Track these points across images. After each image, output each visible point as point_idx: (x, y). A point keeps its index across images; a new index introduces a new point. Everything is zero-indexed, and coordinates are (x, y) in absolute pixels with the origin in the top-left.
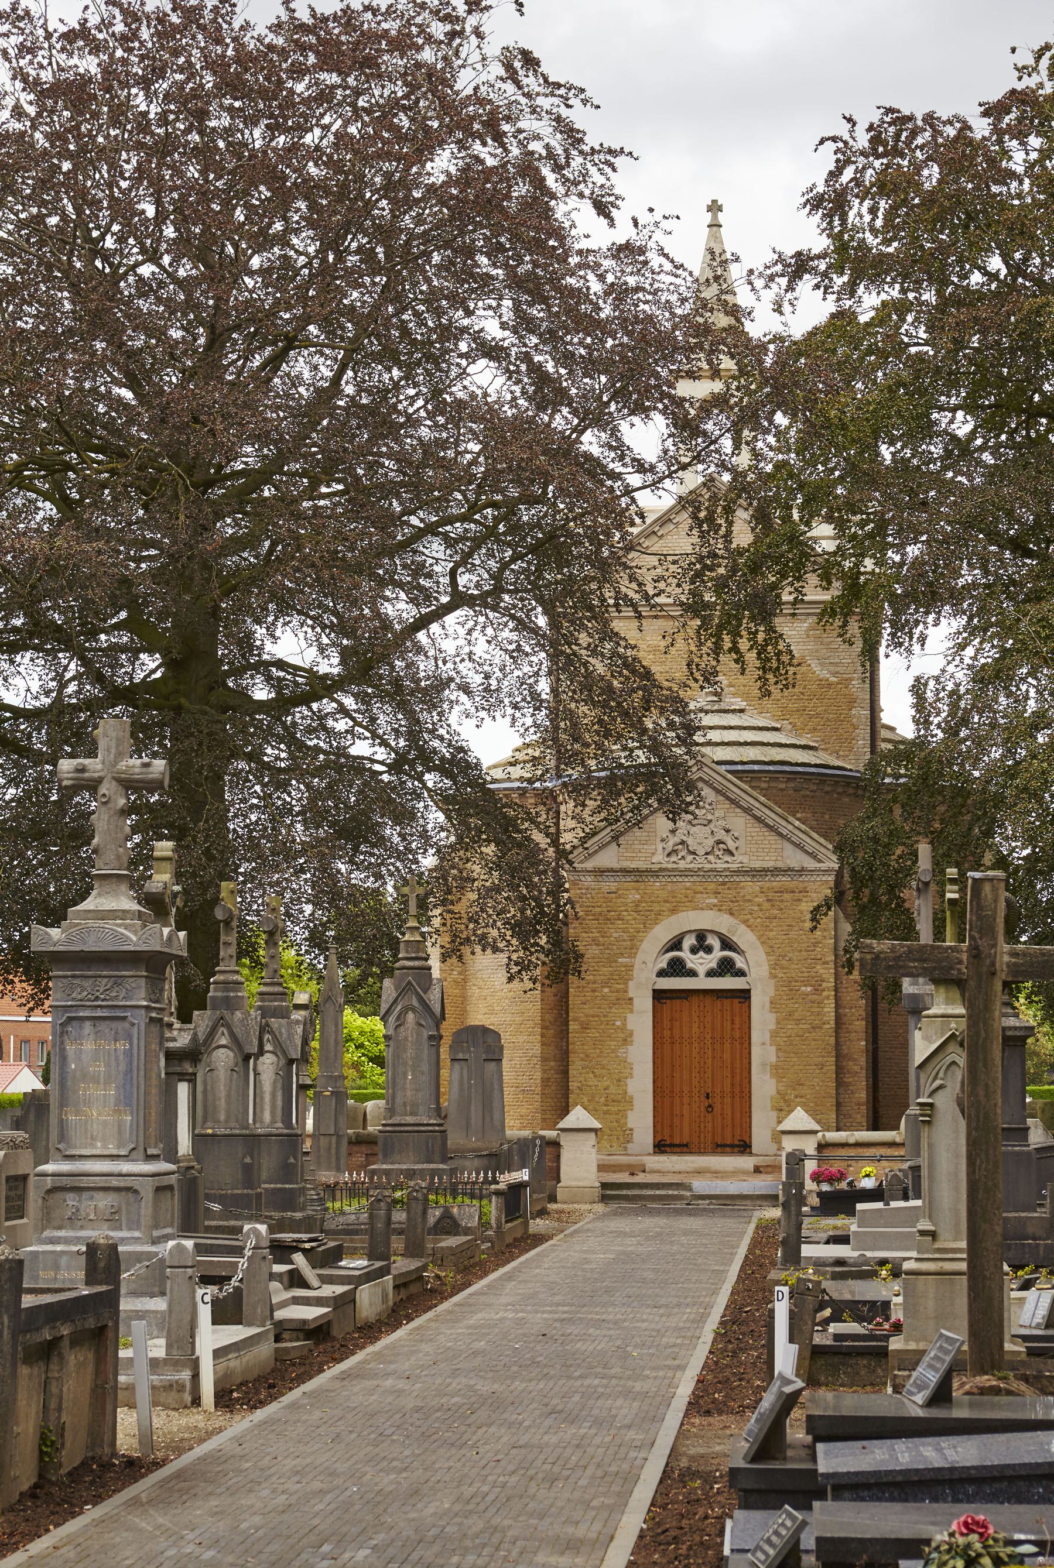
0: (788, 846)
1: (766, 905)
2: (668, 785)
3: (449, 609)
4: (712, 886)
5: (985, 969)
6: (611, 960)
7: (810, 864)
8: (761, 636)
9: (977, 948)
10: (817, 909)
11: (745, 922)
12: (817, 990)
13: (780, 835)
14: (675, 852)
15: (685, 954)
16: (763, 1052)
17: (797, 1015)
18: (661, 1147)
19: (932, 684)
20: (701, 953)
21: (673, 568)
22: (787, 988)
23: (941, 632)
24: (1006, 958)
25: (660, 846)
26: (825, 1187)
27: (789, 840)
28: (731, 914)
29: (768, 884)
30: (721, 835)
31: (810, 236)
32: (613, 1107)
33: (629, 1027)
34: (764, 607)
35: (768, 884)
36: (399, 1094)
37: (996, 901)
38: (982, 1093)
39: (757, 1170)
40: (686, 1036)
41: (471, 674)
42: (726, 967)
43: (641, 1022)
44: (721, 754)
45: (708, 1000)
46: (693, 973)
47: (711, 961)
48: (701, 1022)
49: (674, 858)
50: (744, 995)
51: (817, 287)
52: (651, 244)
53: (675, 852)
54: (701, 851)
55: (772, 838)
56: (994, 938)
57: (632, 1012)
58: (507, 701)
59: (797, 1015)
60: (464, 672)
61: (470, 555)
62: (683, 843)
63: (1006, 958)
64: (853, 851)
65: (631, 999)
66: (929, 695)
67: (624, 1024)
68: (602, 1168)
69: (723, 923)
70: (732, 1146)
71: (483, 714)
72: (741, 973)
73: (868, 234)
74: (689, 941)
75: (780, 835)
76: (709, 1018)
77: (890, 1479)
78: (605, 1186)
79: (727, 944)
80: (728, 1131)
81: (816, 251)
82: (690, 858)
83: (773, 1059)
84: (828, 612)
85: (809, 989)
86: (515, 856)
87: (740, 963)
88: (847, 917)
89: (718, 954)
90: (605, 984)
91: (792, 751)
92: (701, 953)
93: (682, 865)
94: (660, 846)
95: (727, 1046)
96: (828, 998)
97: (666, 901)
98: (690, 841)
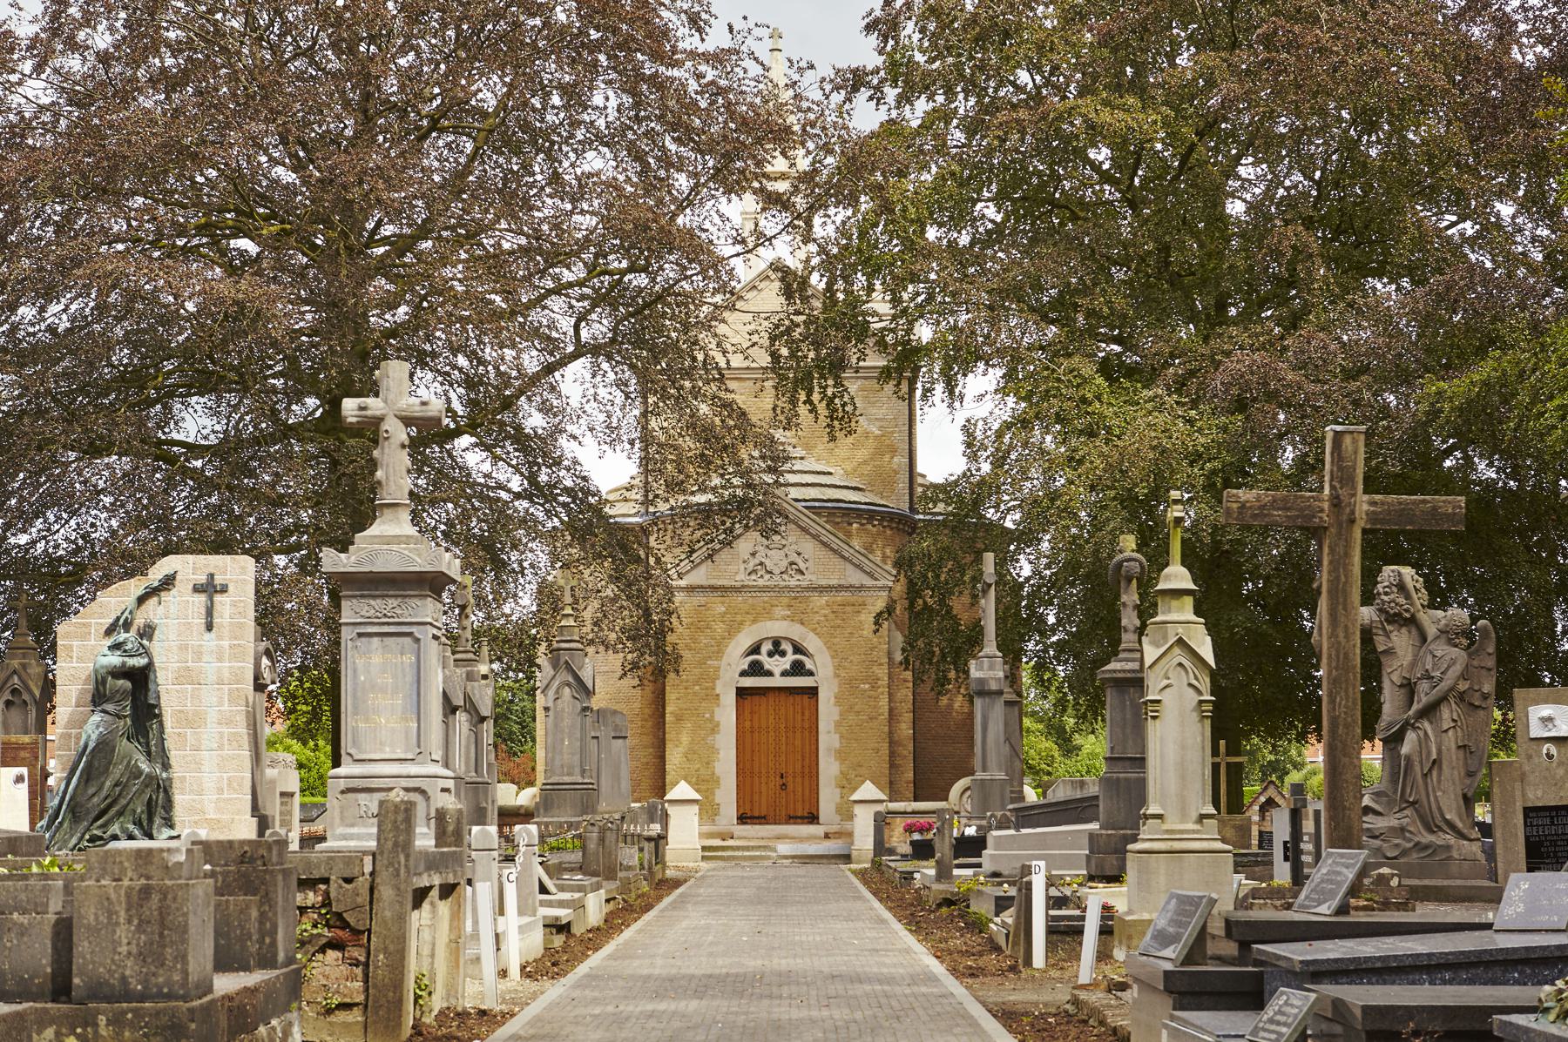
0: (850, 567)
1: (832, 616)
2: (754, 511)
3: (575, 356)
4: (786, 600)
5: (1345, 517)
6: (702, 663)
7: (869, 582)
8: (830, 392)
9: (1337, 497)
10: (879, 615)
11: (814, 630)
12: (874, 687)
13: (843, 557)
14: (755, 571)
16: (828, 738)
17: (857, 708)
18: (743, 819)
19: (980, 423)
21: (766, 323)
22: (849, 687)
23: (981, 382)
24: (1365, 507)
25: (742, 567)
26: (916, 837)
27: (850, 561)
30: (794, 557)
31: (867, 54)
32: (706, 784)
34: (836, 366)
36: (558, 757)
37: (1356, 453)
38: (1342, 635)
39: (827, 836)
40: (764, 725)
41: (596, 413)
42: (797, 669)
43: (727, 713)
44: (794, 493)
45: (783, 697)
46: (769, 674)
47: (785, 663)
48: (777, 714)
49: (753, 577)
50: (813, 692)
51: (871, 98)
52: (744, 48)
53: (755, 571)
54: (777, 571)
55: (836, 560)
56: (1354, 488)
58: (625, 438)
59: (857, 708)
60: (589, 411)
61: (589, 312)
62: (761, 564)
63: (1365, 507)
64: (911, 566)
66: (978, 433)
67: (712, 716)
68: (701, 835)
69: (795, 631)
70: (802, 818)
71: (605, 447)
72: (811, 674)
73: (916, 53)
75: (843, 557)
76: (783, 711)
77: (1370, 965)
78: (704, 848)
79: (798, 649)
80: (799, 806)
81: (870, 68)
82: (767, 577)
83: (837, 745)
84: (885, 374)
86: (632, 570)
87: (809, 665)
88: (898, 628)
89: (791, 657)
90: (697, 683)
91: (845, 492)
93: (761, 582)
94: (742, 567)
95: (798, 735)
98: (767, 562)
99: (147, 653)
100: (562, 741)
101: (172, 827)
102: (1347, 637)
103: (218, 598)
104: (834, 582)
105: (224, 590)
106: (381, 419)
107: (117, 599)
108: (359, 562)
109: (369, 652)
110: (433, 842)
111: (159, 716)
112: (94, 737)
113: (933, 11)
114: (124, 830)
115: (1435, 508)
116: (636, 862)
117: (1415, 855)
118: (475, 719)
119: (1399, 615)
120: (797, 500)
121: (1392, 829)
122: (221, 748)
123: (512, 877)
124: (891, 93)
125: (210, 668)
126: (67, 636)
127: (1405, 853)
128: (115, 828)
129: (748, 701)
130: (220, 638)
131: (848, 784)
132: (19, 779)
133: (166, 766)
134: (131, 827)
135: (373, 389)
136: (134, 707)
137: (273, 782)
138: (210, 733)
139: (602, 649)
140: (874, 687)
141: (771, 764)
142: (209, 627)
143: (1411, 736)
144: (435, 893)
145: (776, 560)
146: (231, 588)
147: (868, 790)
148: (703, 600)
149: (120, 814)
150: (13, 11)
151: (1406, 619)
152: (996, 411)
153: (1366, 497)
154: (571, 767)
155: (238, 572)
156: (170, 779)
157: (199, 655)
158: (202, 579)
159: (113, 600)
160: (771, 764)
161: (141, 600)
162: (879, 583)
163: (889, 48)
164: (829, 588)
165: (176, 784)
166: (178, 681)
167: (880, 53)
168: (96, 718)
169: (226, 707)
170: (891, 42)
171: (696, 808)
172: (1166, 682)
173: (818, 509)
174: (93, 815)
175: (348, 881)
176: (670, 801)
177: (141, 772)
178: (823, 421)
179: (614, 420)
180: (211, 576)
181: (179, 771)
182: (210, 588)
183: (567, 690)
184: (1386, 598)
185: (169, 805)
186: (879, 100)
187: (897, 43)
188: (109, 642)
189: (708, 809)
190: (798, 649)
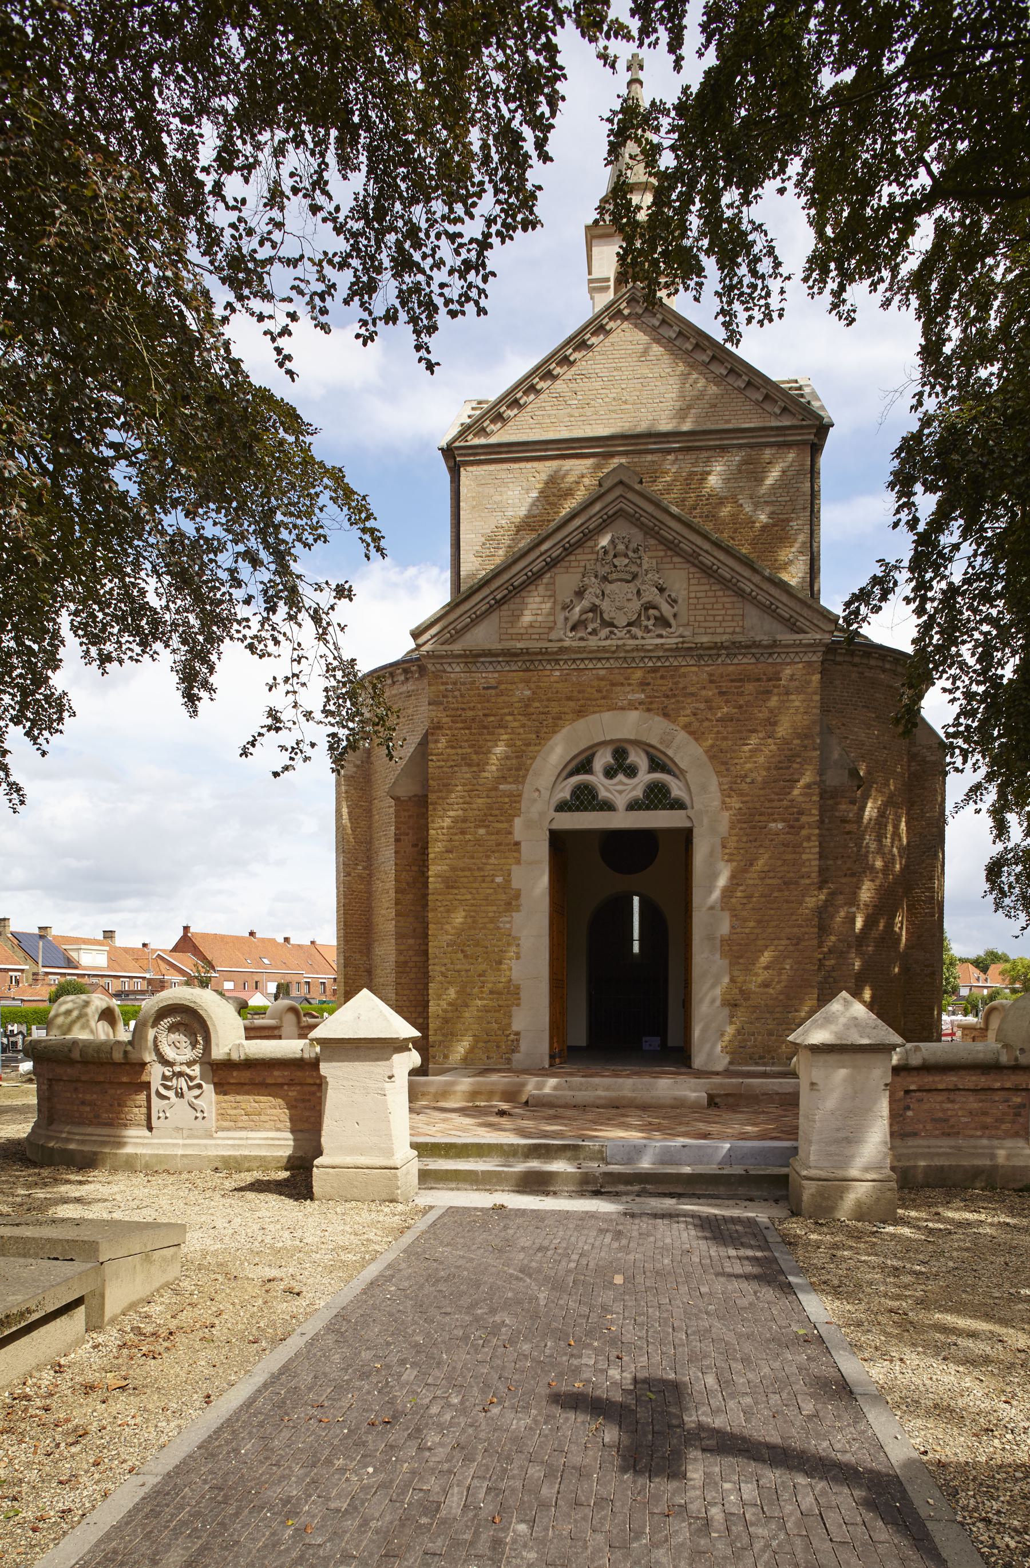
4: (639, 674)
7: (787, 637)
12: (794, 828)
15: (597, 779)
20: (621, 777)
22: (750, 825)
27: (753, 601)
28: (666, 715)
29: (721, 669)
30: (651, 594)
33: (515, 884)
35: (721, 669)
42: (657, 797)
47: (634, 787)
50: (685, 837)
54: (622, 621)
57: (518, 862)
62: (594, 609)
65: (517, 844)
67: (508, 881)
72: (678, 805)
74: (603, 759)
75: (740, 594)
85: (780, 826)
87: (676, 790)
89: (645, 777)
92: (621, 777)
93: (593, 642)
96: (808, 839)
97: (569, 699)
98: (605, 605)
145: (621, 601)
148: (492, 678)
162: (807, 638)
190: (656, 765)
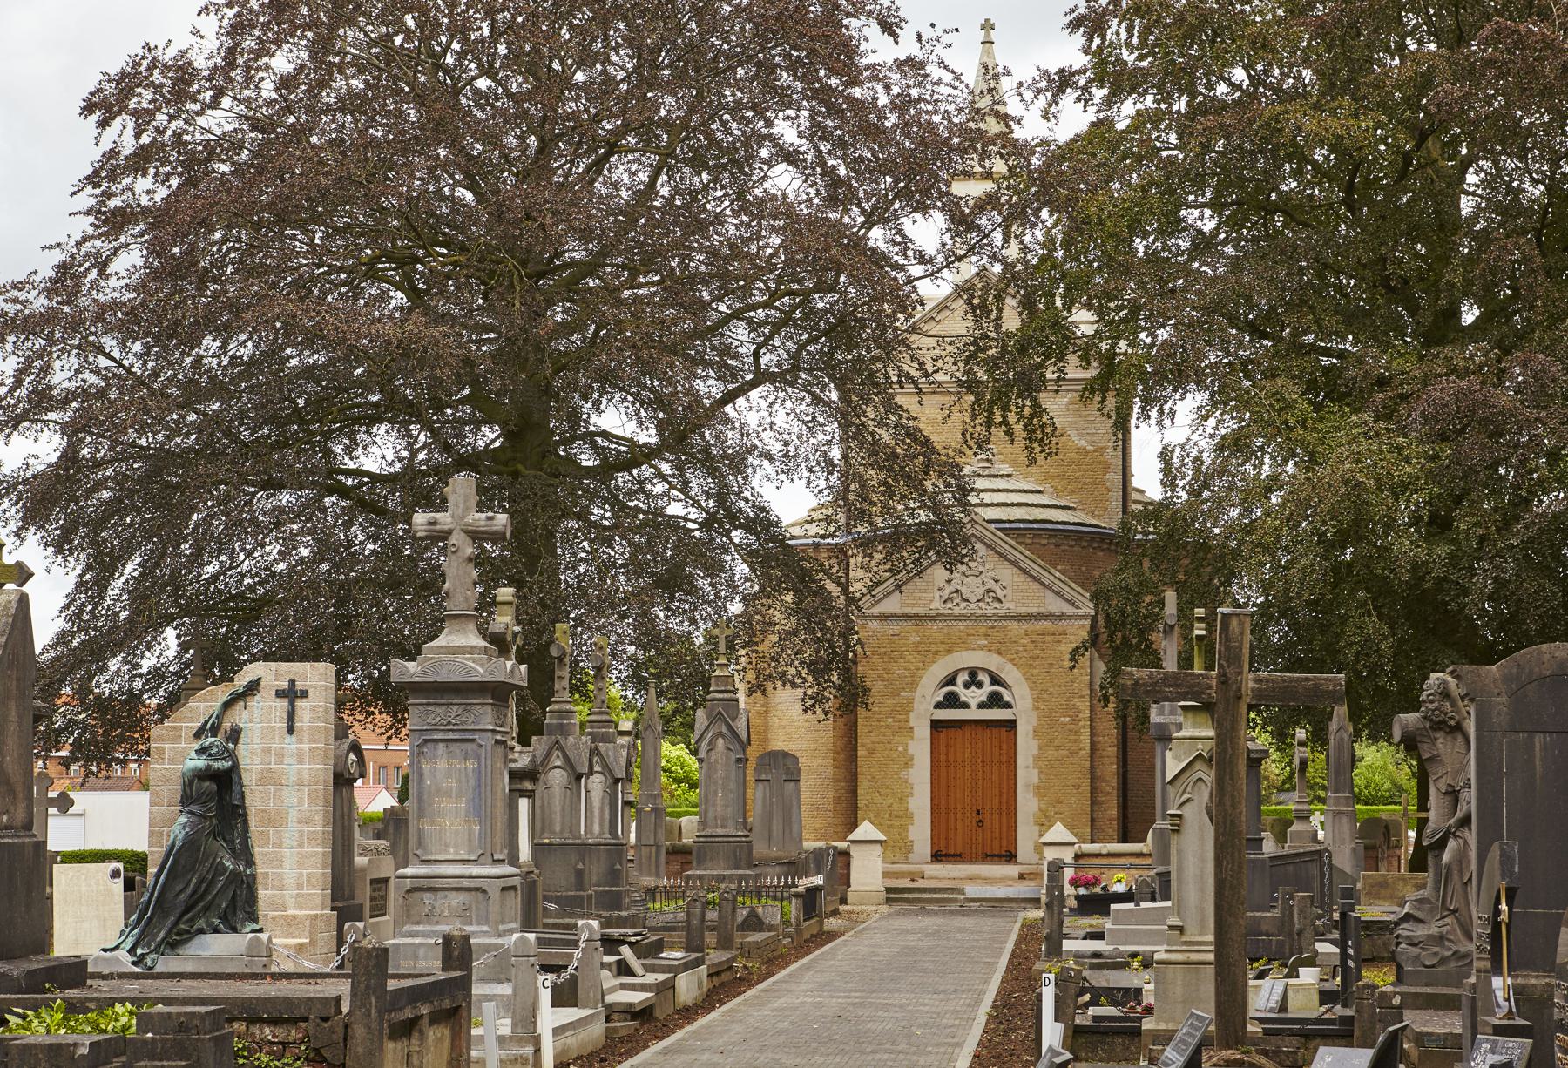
0: (1049, 594)
1: (1030, 646)
2: (945, 540)
3: (753, 385)
4: (983, 629)
6: (894, 694)
7: (1069, 610)
9: (1225, 675)
11: (1012, 661)
12: (1075, 720)
13: (1043, 584)
14: (951, 599)
15: (959, 689)
16: (1027, 774)
17: (1057, 742)
18: (937, 857)
21: (950, 348)
24: (1251, 684)
25: (937, 594)
26: (1082, 891)
30: (991, 584)
31: (1071, 53)
32: (895, 822)
33: (910, 751)
34: (1030, 385)
36: (711, 809)
38: (1228, 803)
41: (772, 441)
42: (995, 701)
43: (920, 747)
44: (991, 513)
45: (979, 730)
46: (966, 706)
47: (981, 695)
48: (973, 749)
49: (949, 605)
50: (1011, 725)
51: (1078, 100)
53: (951, 599)
55: (1036, 587)
59: (1057, 742)
62: (957, 591)
63: (1251, 684)
64: (1108, 599)
66: (1175, 460)
68: (886, 875)
69: (993, 662)
70: (1000, 856)
71: (783, 477)
72: (1008, 706)
73: (1124, 51)
74: (963, 678)
75: (1043, 584)
76: (980, 745)
78: (888, 890)
79: (995, 680)
80: (996, 844)
82: (963, 604)
83: (1036, 781)
87: (1007, 697)
88: (1101, 656)
89: (988, 688)
90: (890, 715)
91: (1053, 511)
93: (957, 611)
94: (937, 594)
95: (995, 769)
98: (963, 590)
99: (232, 756)
100: (716, 793)
101: (256, 921)
102: (1233, 805)
103: (299, 703)
104: (1034, 610)
105: (304, 694)
106: (449, 533)
107: (204, 704)
108: (424, 673)
109: (435, 757)
110: (439, 964)
111: (244, 816)
112: (180, 837)
113: (1137, 10)
114: (209, 924)
115: (1316, 686)
116: (777, 920)
117: (1453, 964)
118: (610, 781)
119: (1444, 722)
120: (990, 521)
121: (1431, 937)
122: (301, 846)
123: (547, 983)
124: (1099, 93)
125: (291, 769)
126: (160, 739)
127: (1443, 961)
128: (201, 923)
129: (943, 734)
130: (300, 741)
131: (1044, 824)
132: (115, 874)
133: (250, 863)
134: (216, 921)
135: (442, 506)
136: (220, 807)
137: (363, 870)
138: (291, 832)
139: (779, 684)
140: (1075, 720)
141: (967, 800)
142: (291, 730)
143: (1452, 844)
144: (426, 1021)
146: (311, 693)
147: (1059, 832)
148: (896, 629)
149: (206, 909)
150: (195, 39)
151: (1450, 727)
152: (1195, 437)
153: (1251, 675)
154: (724, 819)
155: (316, 676)
156: (254, 876)
157: (280, 757)
158: (285, 685)
159: (202, 705)
160: (967, 800)
161: (227, 705)
162: (1080, 612)
163: (1094, 47)
164: (1029, 617)
165: (260, 880)
166: (261, 781)
167: (1087, 53)
168: (183, 819)
169: (305, 807)
170: (1097, 41)
171: (878, 849)
172: (1186, 796)
173: (1013, 531)
174: (179, 911)
175: (325, 1019)
176: (853, 842)
177: (225, 869)
178: (1021, 442)
179: (792, 449)
180: (292, 682)
181: (261, 869)
182: (292, 694)
183: (720, 742)
184: (1431, 706)
185: (252, 899)
186: (1086, 101)
187: (1103, 42)
188: (196, 746)
189: (895, 846)
